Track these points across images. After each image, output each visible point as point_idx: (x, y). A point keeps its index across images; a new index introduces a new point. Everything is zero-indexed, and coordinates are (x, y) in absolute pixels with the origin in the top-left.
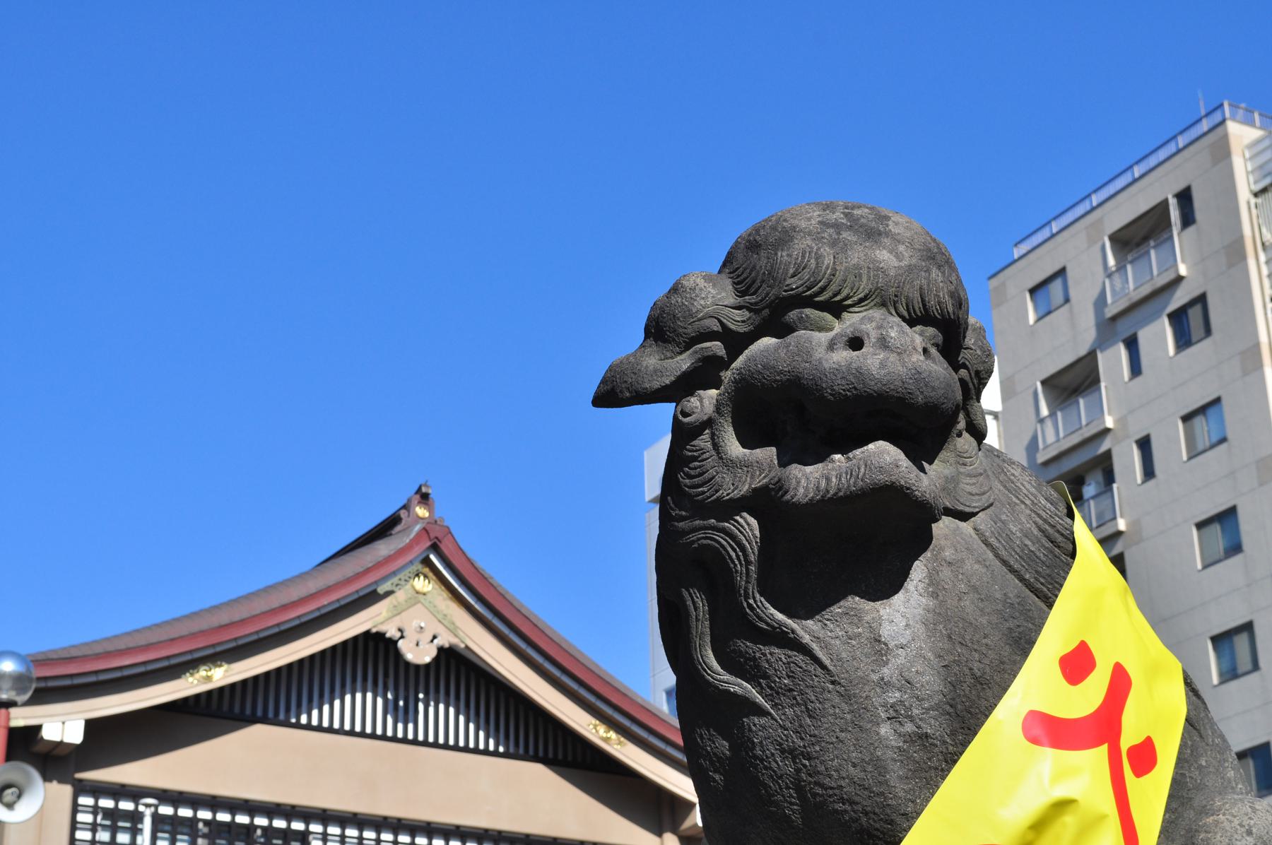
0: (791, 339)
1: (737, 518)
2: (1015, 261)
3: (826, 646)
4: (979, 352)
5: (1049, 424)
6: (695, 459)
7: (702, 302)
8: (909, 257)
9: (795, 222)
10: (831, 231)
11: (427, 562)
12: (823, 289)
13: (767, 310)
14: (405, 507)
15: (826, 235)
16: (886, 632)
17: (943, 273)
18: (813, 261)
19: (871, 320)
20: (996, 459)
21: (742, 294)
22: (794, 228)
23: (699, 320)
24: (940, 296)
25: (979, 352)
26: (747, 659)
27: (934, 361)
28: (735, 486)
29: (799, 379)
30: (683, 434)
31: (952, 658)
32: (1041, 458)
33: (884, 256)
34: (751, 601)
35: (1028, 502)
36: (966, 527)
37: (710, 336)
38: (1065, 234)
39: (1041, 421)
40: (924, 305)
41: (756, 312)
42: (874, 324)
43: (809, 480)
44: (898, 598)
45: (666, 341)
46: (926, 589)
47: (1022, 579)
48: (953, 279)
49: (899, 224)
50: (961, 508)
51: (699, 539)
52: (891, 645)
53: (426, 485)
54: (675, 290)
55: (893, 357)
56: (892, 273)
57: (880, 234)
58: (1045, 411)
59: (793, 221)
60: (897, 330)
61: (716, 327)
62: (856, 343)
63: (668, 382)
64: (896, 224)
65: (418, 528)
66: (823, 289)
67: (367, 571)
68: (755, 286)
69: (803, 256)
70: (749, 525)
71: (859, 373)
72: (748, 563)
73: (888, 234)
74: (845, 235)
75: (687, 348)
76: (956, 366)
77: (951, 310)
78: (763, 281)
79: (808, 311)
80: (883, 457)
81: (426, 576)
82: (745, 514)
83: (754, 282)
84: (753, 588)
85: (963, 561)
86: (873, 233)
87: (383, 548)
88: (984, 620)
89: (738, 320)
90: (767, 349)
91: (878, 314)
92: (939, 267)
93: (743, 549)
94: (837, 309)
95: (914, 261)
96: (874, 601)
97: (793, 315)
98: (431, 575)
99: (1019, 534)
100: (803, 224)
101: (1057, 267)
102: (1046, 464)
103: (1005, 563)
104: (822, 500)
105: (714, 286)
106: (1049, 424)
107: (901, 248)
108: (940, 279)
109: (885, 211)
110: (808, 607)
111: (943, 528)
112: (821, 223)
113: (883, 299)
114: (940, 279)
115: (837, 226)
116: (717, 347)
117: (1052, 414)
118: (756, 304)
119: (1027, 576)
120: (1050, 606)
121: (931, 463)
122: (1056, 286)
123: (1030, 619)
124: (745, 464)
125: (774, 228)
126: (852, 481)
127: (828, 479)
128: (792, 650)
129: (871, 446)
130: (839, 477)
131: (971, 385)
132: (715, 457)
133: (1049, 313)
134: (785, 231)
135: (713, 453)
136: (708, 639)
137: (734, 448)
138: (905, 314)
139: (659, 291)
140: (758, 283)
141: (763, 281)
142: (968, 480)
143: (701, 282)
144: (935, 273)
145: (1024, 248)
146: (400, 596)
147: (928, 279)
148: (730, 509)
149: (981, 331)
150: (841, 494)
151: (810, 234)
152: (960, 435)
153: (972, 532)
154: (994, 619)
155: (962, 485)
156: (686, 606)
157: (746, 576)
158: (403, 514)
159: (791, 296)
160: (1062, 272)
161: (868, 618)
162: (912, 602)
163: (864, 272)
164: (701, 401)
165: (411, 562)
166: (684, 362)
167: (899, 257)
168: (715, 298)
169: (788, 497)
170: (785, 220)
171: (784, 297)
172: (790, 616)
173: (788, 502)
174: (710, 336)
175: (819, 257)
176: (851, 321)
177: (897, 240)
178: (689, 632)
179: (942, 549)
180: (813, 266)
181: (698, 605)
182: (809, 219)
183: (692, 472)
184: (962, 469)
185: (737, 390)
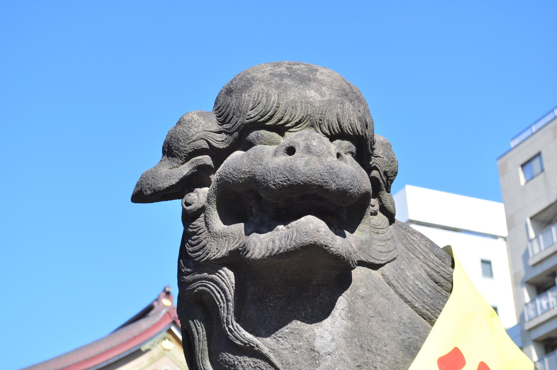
0: (251, 151)
1: (221, 271)
2: (511, 149)
3: (279, 355)
4: (385, 159)
5: (535, 243)
6: (195, 233)
7: (196, 129)
8: (328, 94)
9: (253, 74)
10: (277, 79)
11: (170, 331)
12: (271, 117)
13: (237, 133)
14: (157, 300)
15: (273, 82)
16: (318, 344)
17: (354, 105)
18: (264, 99)
19: (301, 135)
20: (403, 231)
21: (222, 123)
22: (253, 78)
23: (194, 141)
24: (351, 119)
25: (385, 159)
26: (230, 366)
27: (346, 162)
28: (218, 250)
29: (255, 176)
30: (189, 217)
31: (362, 360)
32: (531, 262)
33: (312, 94)
34: (231, 327)
35: (421, 257)
36: (376, 274)
37: (201, 152)
38: (540, 133)
39: (531, 241)
40: (340, 126)
41: (230, 134)
42: (303, 138)
43: (263, 244)
44: (327, 322)
45: (173, 156)
46: (346, 315)
47: (413, 307)
48: (361, 109)
49: (324, 74)
50: (372, 261)
51: (198, 287)
52: (322, 352)
53: (169, 287)
54: (179, 123)
55: (314, 158)
56: (317, 105)
57: (310, 80)
58: (532, 235)
59: (253, 74)
60: (318, 140)
61: (206, 146)
62: (291, 151)
63: (174, 183)
64: (321, 73)
65: (164, 312)
66: (271, 117)
67: (135, 338)
68: (229, 117)
69: (258, 96)
70: (228, 276)
71: (291, 170)
72: (228, 301)
73: (315, 80)
74: (286, 81)
75: (187, 160)
76: (369, 169)
77: (359, 130)
78: (234, 114)
79: (263, 132)
80: (311, 227)
81: (170, 340)
82: (225, 269)
83: (228, 115)
84: (231, 318)
85: (371, 295)
86: (304, 80)
87: (144, 324)
88: (385, 335)
89: (220, 141)
90: (236, 158)
91: (306, 131)
92: (351, 101)
93: (225, 292)
94: (281, 129)
95: (333, 97)
96: (311, 323)
97: (253, 135)
98: (172, 339)
99: (411, 277)
100: (259, 75)
101: (535, 152)
102: (535, 265)
103: (402, 296)
104: (270, 256)
105: (204, 119)
106: (535, 243)
107: (324, 89)
108: (351, 108)
109: (315, 66)
110: (265, 329)
111: (358, 273)
112: (270, 74)
113: (314, 124)
114: (351, 108)
115: (281, 76)
116: (207, 159)
117: (537, 237)
118: (230, 129)
119: (417, 305)
120: (432, 324)
121: (352, 232)
122: (536, 162)
123: (418, 333)
124: (224, 236)
125: (241, 79)
126: (288, 242)
127: (273, 242)
128: (257, 358)
129: (303, 219)
130: (280, 240)
131: (381, 181)
132: (207, 232)
133: (532, 178)
134: (248, 80)
135: (205, 229)
136: (206, 353)
137: (217, 224)
138: (328, 132)
139: (169, 125)
140: (231, 115)
141: (234, 114)
142: (380, 243)
143: (196, 117)
144: (347, 105)
145: (517, 141)
146: (155, 352)
147: (342, 108)
148: (215, 265)
149: (387, 146)
150: (281, 251)
151: (263, 81)
152: (375, 214)
153: (381, 277)
154: (392, 333)
155: (374, 246)
156: (192, 332)
157: (227, 311)
158: (155, 304)
159: (251, 122)
160: (539, 155)
161: (306, 335)
162: (337, 323)
163: (299, 104)
164: (198, 195)
165: (160, 332)
166: (185, 169)
167: (322, 94)
168: (205, 127)
169: (248, 255)
170: (248, 74)
171: (247, 124)
172: (256, 335)
173: (249, 258)
174: (201, 152)
175: (268, 96)
176: (290, 137)
177: (321, 83)
178: (195, 349)
179: (357, 288)
180: (265, 102)
181: (200, 331)
182: (263, 72)
183: (193, 243)
184: (376, 236)
185: (218, 186)
